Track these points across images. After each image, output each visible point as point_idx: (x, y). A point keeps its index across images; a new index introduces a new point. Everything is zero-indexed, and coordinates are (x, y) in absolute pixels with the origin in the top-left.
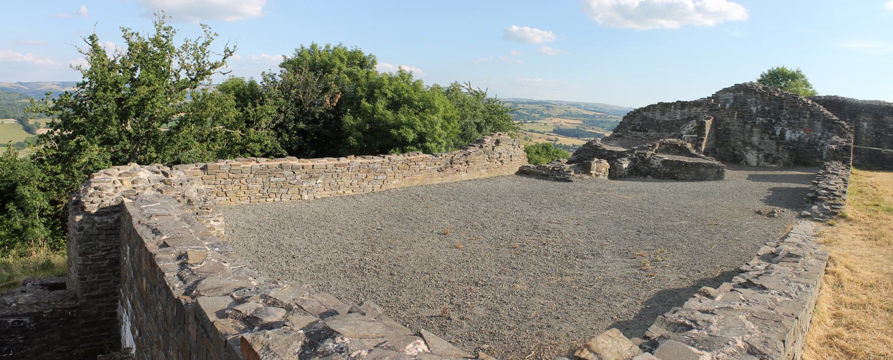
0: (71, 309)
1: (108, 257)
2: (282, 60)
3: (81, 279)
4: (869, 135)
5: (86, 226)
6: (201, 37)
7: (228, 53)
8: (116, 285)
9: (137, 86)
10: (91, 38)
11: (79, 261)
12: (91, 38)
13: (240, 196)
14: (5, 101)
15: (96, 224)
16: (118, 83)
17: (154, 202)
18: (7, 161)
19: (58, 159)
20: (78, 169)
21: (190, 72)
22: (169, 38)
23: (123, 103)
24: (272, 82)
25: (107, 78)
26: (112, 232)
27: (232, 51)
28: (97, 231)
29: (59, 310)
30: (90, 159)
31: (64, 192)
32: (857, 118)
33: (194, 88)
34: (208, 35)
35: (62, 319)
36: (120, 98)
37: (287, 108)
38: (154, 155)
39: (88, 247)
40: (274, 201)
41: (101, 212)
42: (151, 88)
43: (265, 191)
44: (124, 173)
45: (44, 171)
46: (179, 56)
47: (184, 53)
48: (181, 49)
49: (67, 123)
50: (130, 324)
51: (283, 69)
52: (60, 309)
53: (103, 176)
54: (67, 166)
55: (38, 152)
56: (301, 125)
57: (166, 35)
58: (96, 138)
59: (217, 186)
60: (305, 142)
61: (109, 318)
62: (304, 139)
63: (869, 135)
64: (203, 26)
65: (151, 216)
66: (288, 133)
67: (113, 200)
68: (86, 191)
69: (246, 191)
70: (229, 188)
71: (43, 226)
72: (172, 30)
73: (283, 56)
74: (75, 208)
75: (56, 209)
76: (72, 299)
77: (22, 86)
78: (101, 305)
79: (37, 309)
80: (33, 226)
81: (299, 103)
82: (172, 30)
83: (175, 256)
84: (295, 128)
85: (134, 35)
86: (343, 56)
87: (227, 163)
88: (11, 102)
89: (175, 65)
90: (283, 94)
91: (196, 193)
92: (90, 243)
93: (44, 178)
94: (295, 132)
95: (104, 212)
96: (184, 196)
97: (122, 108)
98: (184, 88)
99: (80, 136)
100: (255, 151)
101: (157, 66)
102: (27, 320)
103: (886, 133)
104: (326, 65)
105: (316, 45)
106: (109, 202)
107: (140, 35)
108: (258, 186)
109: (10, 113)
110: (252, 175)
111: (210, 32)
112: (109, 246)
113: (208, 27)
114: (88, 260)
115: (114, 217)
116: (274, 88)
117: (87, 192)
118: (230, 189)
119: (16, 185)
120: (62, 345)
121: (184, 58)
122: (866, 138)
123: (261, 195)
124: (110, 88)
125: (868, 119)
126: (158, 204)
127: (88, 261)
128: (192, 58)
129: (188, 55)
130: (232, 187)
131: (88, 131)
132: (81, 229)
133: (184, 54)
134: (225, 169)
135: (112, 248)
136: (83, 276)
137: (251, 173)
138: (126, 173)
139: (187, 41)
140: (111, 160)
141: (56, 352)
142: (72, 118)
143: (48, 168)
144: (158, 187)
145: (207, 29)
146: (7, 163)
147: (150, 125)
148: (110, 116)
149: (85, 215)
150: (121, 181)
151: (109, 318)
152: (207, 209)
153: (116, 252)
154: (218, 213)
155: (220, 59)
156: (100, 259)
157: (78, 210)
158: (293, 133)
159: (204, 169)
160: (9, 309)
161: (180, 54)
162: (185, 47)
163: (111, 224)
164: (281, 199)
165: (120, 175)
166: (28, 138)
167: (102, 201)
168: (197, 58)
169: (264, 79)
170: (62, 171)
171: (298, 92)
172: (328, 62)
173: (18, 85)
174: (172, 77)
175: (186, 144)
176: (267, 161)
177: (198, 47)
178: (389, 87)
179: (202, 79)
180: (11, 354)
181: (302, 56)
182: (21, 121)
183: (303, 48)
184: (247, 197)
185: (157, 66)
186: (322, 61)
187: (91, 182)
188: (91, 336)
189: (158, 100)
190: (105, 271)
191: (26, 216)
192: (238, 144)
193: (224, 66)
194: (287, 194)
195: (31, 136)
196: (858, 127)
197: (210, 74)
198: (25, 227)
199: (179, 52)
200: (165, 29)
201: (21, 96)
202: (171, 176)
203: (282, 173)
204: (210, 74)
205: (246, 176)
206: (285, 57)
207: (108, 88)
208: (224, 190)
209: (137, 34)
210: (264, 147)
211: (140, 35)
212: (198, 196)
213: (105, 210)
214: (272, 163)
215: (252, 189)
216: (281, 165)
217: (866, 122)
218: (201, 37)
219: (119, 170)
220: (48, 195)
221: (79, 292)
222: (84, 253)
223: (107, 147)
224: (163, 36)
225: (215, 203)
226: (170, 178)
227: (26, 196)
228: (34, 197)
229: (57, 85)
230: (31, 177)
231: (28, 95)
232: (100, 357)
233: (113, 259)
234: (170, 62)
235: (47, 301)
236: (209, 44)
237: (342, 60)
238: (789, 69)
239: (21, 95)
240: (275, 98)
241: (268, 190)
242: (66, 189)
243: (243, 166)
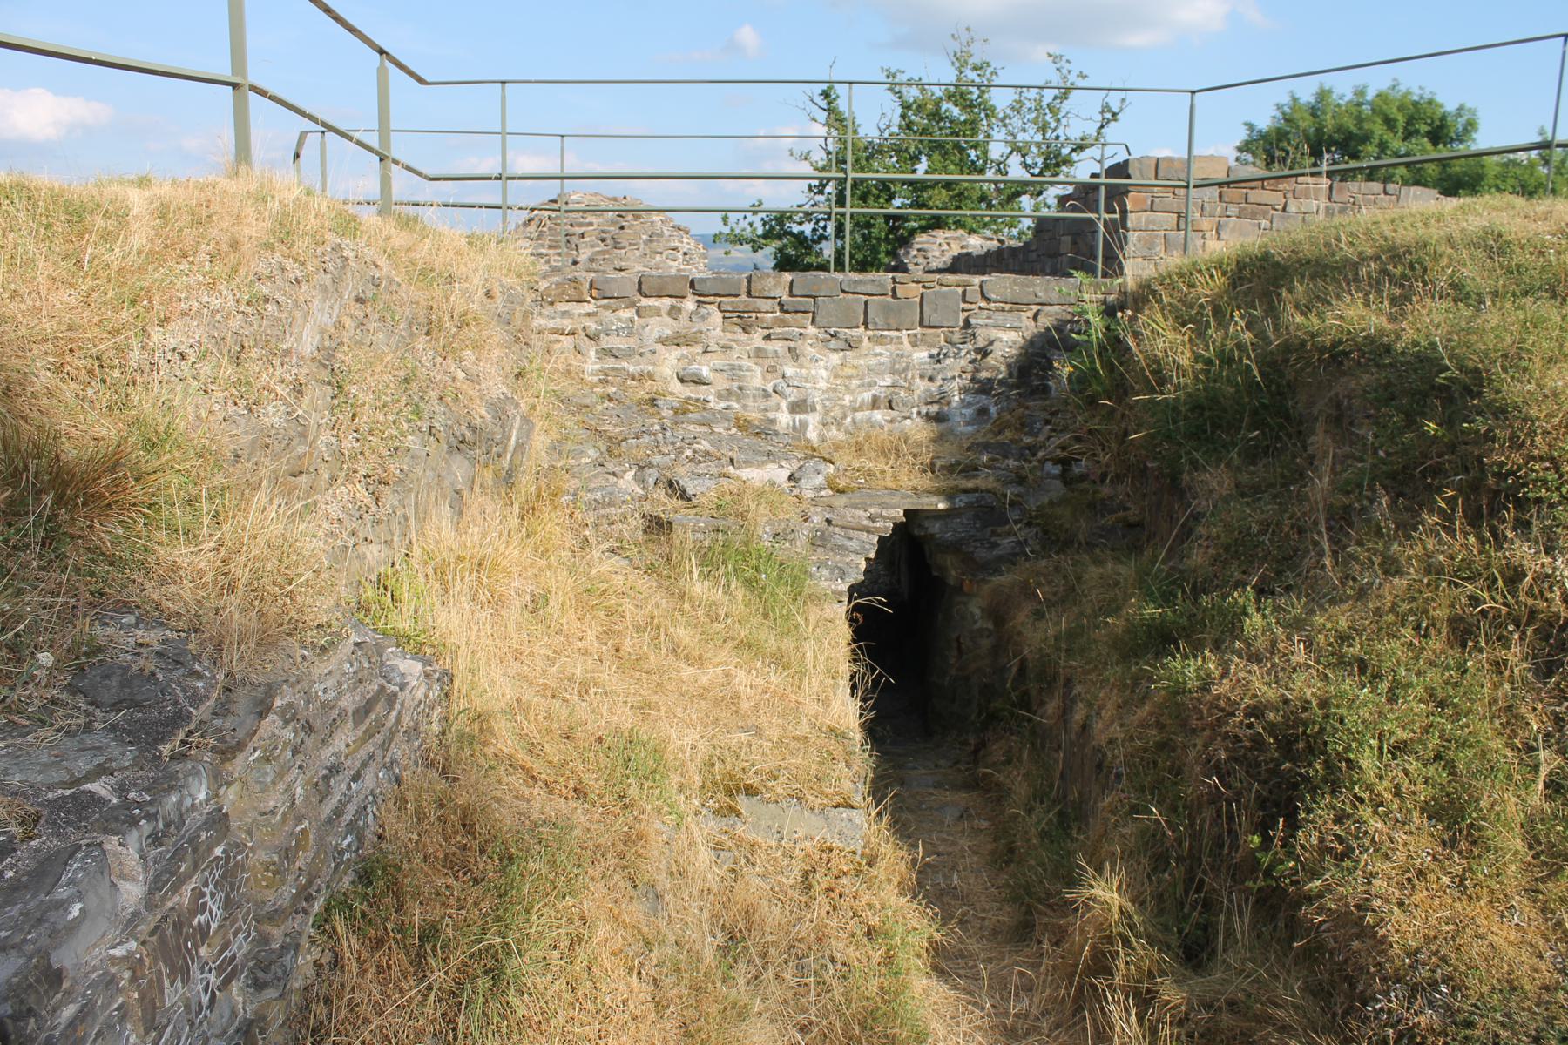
2: (1242, 135)
7: (1110, 116)
21: (1029, 161)
27: (1116, 110)
46: (1005, 126)
47: (1015, 119)
48: (1008, 111)
64: (1055, 59)
72: (990, 70)
73: (1246, 124)
86: (1393, 112)
89: (996, 150)
98: (1018, 194)
104: (1349, 136)
105: (1330, 92)
113: (1064, 59)
124: (876, 192)
133: (1016, 122)
145: (1063, 63)
150: (948, 244)
155: (1091, 130)
168: (1043, 129)
172: (1355, 130)
177: (1044, 104)
178: (1499, 182)
183: (1295, 100)
186: (1340, 129)
199: (1006, 116)
200: (975, 68)
206: (1250, 127)
237: (1389, 123)
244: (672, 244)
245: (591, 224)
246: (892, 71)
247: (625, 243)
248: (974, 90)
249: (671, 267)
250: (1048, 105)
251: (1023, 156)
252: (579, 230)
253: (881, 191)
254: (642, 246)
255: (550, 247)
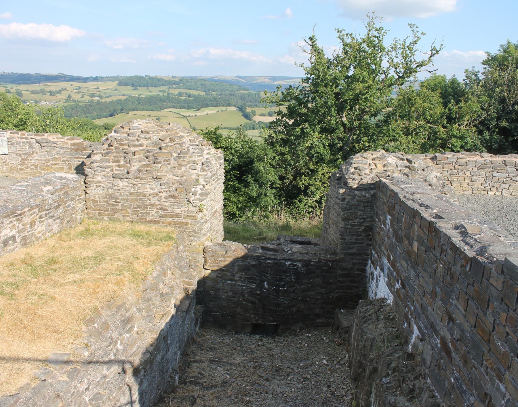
0: (332, 261)
1: (364, 224)
2: (485, 57)
3: (341, 239)
5: (348, 198)
6: (409, 37)
7: (435, 52)
8: (367, 247)
9: (351, 83)
10: (311, 39)
11: (342, 225)
12: (311, 39)
13: (464, 186)
14: (228, 92)
15: (357, 197)
16: (337, 79)
17: (409, 184)
18: (245, 141)
19: (285, 142)
20: (302, 151)
21: (398, 70)
22: (381, 38)
23: (340, 97)
24: (474, 80)
25: (326, 75)
26: (369, 204)
27: (438, 49)
28: (357, 202)
29: (323, 261)
30: (312, 144)
31: (290, 170)
33: (401, 85)
34: (416, 34)
35: (324, 268)
36: (338, 92)
37: (490, 106)
38: (367, 144)
39: (349, 214)
40: (495, 194)
41: (360, 187)
42: (366, 85)
43: (487, 184)
44: (376, 157)
45: (275, 151)
46: (388, 55)
47: (393, 52)
48: (390, 49)
49: (292, 112)
50: (386, 279)
51: (486, 66)
52: (324, 260)
53: (360, 159)
54: (293, 149)
55: (270, 135)
56: (504, 123)
57: (377, 35)
58: (317, 126)
59: (443, 175)
60: (507, 141)
61: (360, 272)
62: (506, 138)
65: (414, 193)
66: (489, 131)
67: (369, 179)
68: (348, 170)
69: (470, 182)
70: (455, 178)
71: (273, 196)
72: (383, 31)
73: (486, 53)
74: (338, 183)
75: (283, 184)
76: (333, 254)
77: (240, 79)
78: (355, 261)
79: (307, 258)
80: (266, 195)
81: (502, 101)
82: (383, 31)
83: (452, 226)
84: (497, 126)
85: (349, 36)
87: (453, 155)
88: (232, 93)
89: (385, 64)
90: (486, 92)
91: (435, 179)
92: (351, 211)
93: (274, 157)
94: (497, 130)
95: (362, 188)
96: (426, 181)
97: (338, 101)
99: (304, 125)
100: (455, 147)
101: (369, 65)
102: (299, 264)
106: (367, 180)
107: (353, 36)
108: (481, 179)
109: (232, 102)
110: (476, 169)
111: (417, 32)
112: (366, 216)
113: (415, 26)
114: (349, 225)
115: (370, 193)
116: (477, 86)
117: (349, 170)
118: (455, 179)
119: (252, 162)
120: (322, 288)
121: (393, 57)
123: (483, 187)
124: (331, 84)
126: (413, 185)
127: (348, 225)
128: (400, 57)
129: (397, 54)
130: (457, 177)
131: (311, 120)
132: (344, 200)
133: (394, 53)
134: (452, 160)
135: (368, 217)
136: (343, 236)
137: (475, 167)
138: (378, 158)
139: (396, 41)
140: (328, 146)
141: (317, 292)
142: (298, 108)
143: (278, 150)
144: (405, 171)
146: (245, 143)
147: (361, 117)
148: (329, 108)
149: (347, 189)
150: (375, 164)
151: (360, 272)
152: (445, 194)
153: (370, 221)
154: (454, 198)
155: (426, 57)
156: (358, 225)
157: (341, 184)
158: (494, 131)
159: (434, 159)
160: (287, 255)
161: (390, 53)
162: (394, 48)
163: (368, 198)
164: (502, 193)
165: (373, 159)
166: (246, 123)
167: (361, 179)
168: (405, 57)
169: (467, 77)
170: (289, 152)
171: (502, 90)
173: (237, 79)
175: (395, 136)
176: (491, 156)
177: (406, 46)
179: (409, 76)
180: (285, 289)
181: (508, 52)
182: (241, 109)
183: (509, 43)
184: (470, 188)
185: (369, 65)
187: (352, 163)
188: (344, 284)
189: (371, 96)
190: (360, 235)
191: (260, 187)
192: (440, 139)
193: (431, 64)
194: (508, 189)
195: (248, 121)
197: (416, 72)
198: (260, 195)
200: (376, 30)
201: (240, 88)
202: (414, 163)
203: (505, 169)
204: (416, 72)
205: (470, 169)
206: (488, 53)
207: (328, 84)
208: (450, 180)
209: (351, 35)
210: (464, 144)
211: (353, 36)
212: (438, 182)
213: (363, 186)
214: (495, 159)
215: (476, 181)
216: (505, 161)
218: (409, 37)
219: (372, 155)
220: (278, 171)
221: (339, 249)
222: (346, 218)
223: (325, 135)
224: (375, 37)
225: (451, 190)
226: (413, 164)
227: (261, 170)
228: (268, 172)
229: (268, 79)
230: (265, 156)
231: (246, 87)
232: (362, 302)
233: (368, 226)
234: (381, 60)
235: (313, 252)
236: (416, 44)
239: (240, 87)
240: (479, 96)
241: (490, 184)
242: (291, 167)
243: (468, 159)
244: (194, 159)
245: (141, 145)
246: (340, 30)
247: (161, 159)
248: (376, 39)
249: (192, 174)
250: (408, 46)
251: (396, 69)
252: (133, 149)
253: (333, 83)
254: (172, 162)
255: (113, 161)
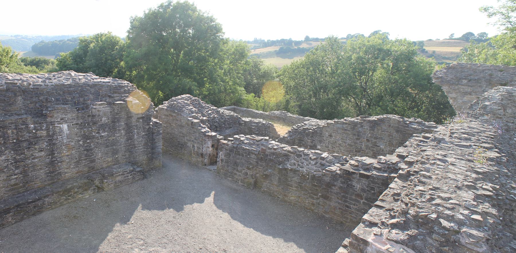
4: (73, 144)
32: (49, 119)
63: (73, 144)
103: (98, 133)
122: (69, 150)
125: (69, 116)
155: (499, 16)
174: (396, 179)
196: (54, 134)
217: (66, 122)
238: (392, 37)
